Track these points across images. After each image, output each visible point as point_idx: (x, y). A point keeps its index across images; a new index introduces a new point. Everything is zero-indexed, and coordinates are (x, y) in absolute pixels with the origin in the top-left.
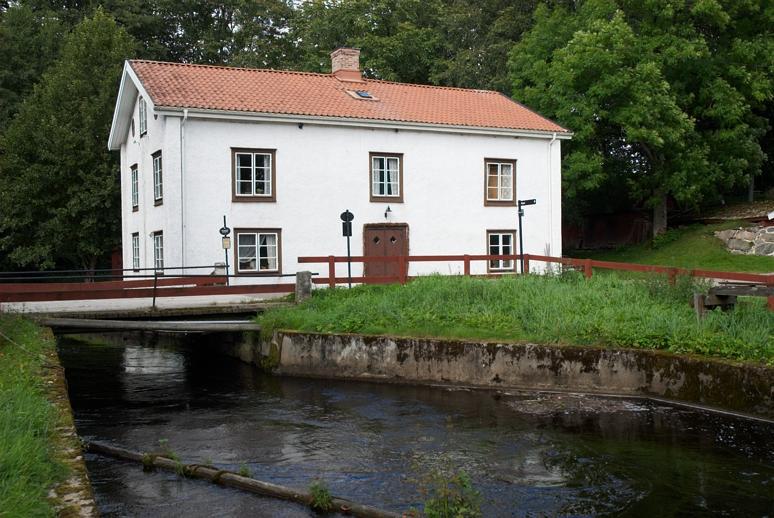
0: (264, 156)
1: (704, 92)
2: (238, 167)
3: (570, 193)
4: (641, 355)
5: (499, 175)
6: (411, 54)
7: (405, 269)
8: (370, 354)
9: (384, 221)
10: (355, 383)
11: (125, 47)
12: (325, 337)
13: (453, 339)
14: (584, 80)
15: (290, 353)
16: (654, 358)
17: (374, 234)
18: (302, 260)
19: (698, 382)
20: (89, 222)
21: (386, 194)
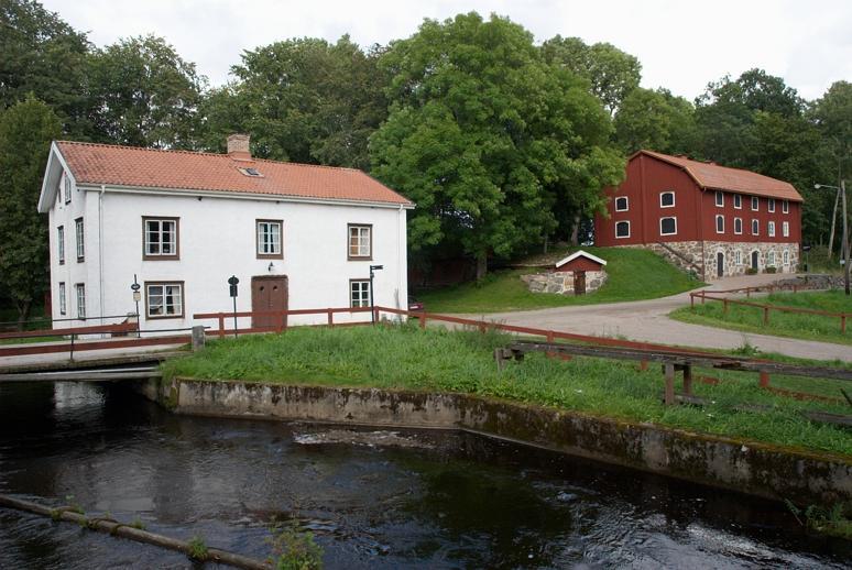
0: (170, 223)
1: (513, 175)
2: (148, 232)
3: (416, 247)
4: (457, 398)
5: (359, 237)
6: (296, 134)
7: (285, 320)
8: (251, 397)
9: (267, 273)
10: (238, 421)
11: (53, 127)
12: (214, 384)
13: (315, 385)
14: (426, 162)
15: (186, 397)
16: (466, 400)
17: (261, 283)
18: (196, 317)
19: (496, 418)
20: (17, 274)
21: (269, 252)
